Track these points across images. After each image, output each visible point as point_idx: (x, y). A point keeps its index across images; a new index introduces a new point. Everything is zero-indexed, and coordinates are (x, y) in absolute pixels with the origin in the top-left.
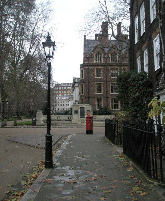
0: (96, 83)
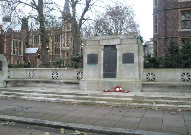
0: (179, 10)
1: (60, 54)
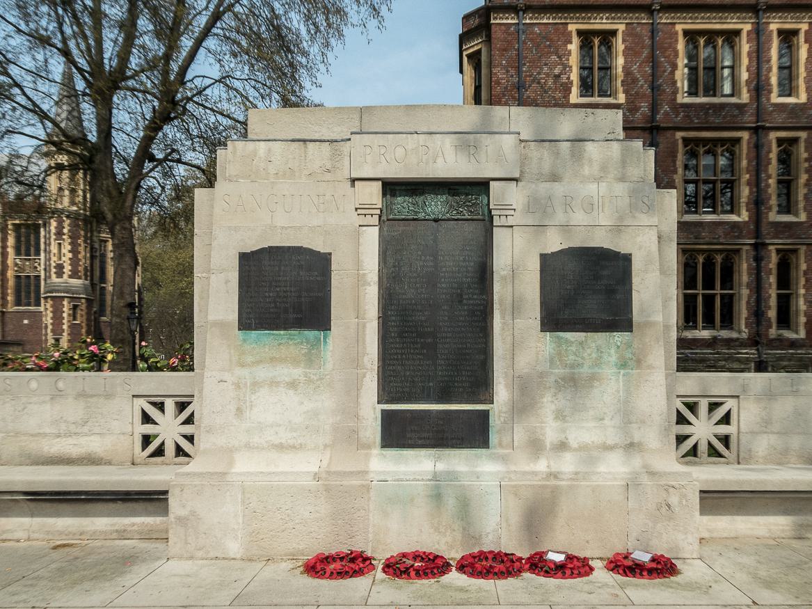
1: (42, 309)
